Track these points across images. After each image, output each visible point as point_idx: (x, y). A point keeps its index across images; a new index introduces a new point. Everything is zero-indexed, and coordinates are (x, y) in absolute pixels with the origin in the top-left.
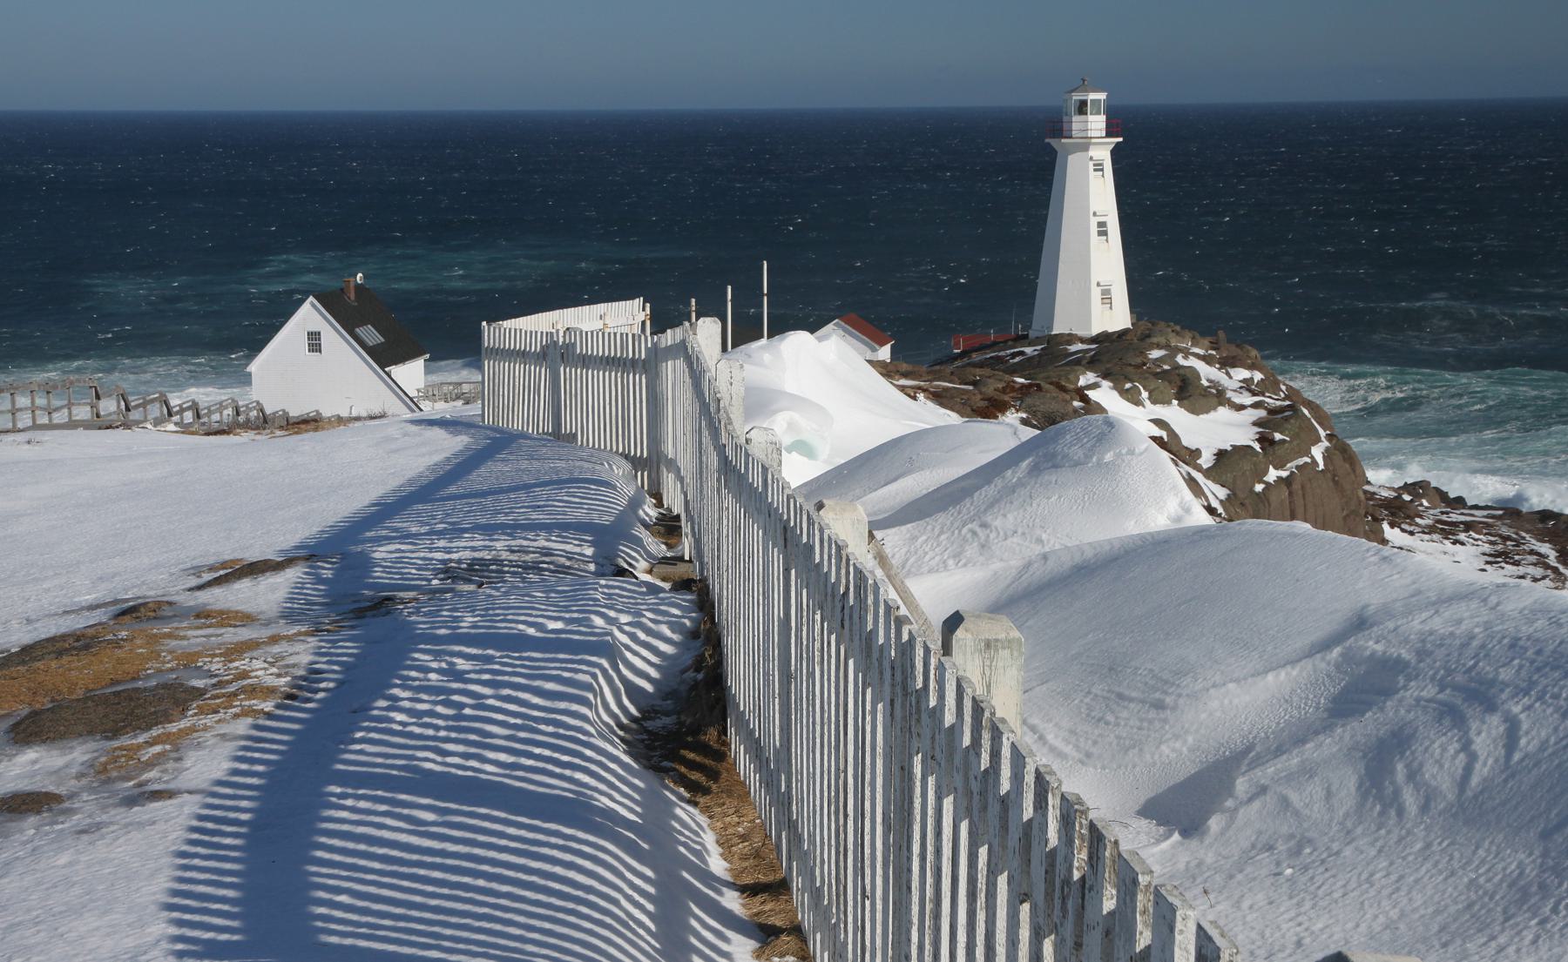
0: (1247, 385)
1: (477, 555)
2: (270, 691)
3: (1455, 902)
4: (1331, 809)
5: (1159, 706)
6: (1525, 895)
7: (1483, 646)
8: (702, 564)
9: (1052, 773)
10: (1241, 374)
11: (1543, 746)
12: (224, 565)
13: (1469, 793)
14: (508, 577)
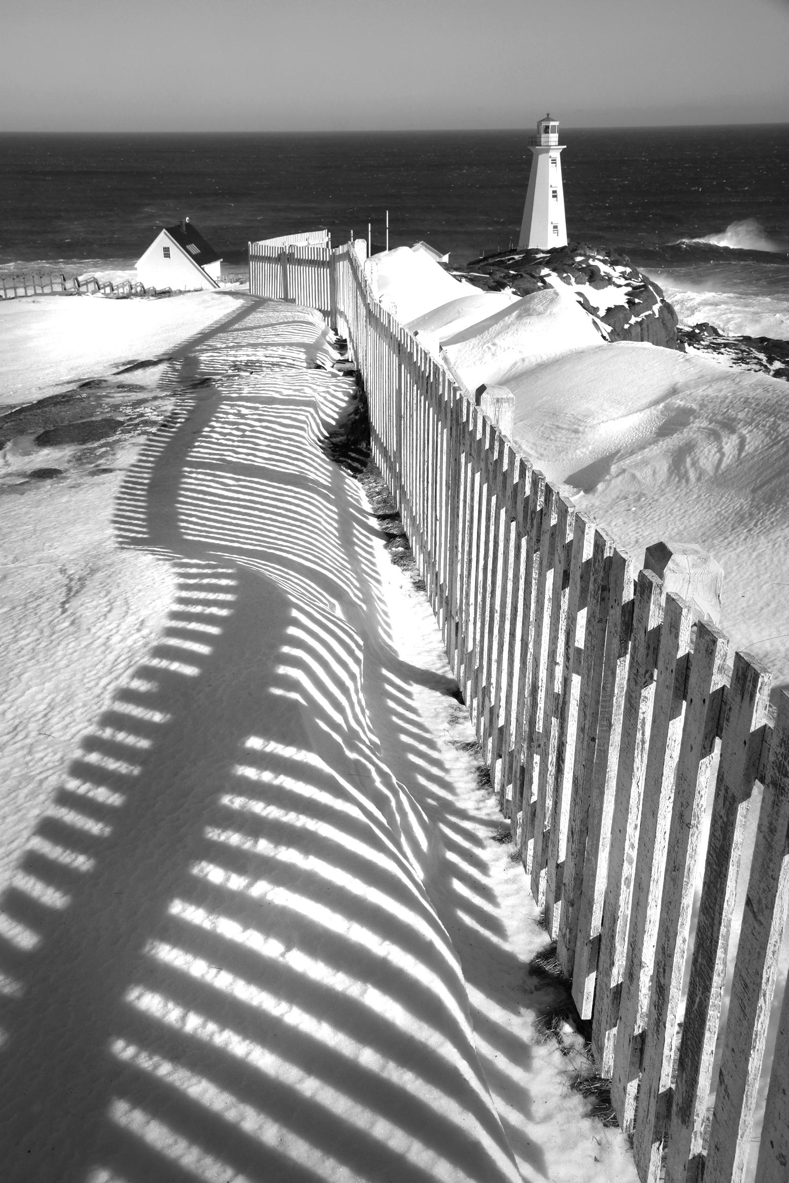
0: (623, 273)
1: (250, 358)
2: (154, 423)
3: (710, 522)
4: (655, 480)
5: (576, 431)
6: (742, 518)
7: (731, 402)
8: (358, 363)
9: (528, 461)
10: (620, 269)
11: (756, 449)
12: (129, 363)
13: (720, 472)
14: (264, 369)
